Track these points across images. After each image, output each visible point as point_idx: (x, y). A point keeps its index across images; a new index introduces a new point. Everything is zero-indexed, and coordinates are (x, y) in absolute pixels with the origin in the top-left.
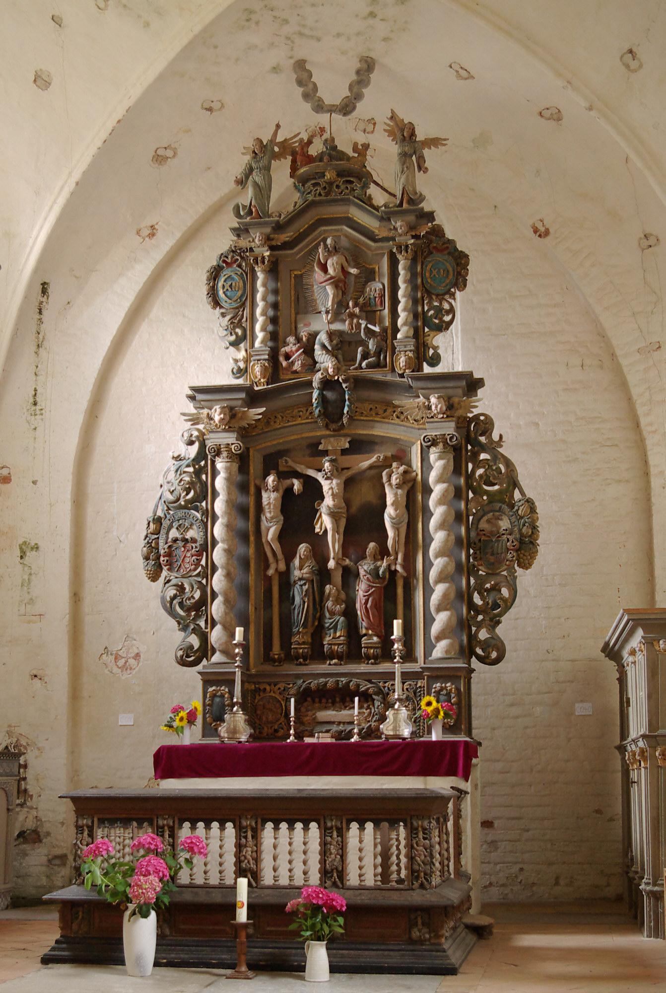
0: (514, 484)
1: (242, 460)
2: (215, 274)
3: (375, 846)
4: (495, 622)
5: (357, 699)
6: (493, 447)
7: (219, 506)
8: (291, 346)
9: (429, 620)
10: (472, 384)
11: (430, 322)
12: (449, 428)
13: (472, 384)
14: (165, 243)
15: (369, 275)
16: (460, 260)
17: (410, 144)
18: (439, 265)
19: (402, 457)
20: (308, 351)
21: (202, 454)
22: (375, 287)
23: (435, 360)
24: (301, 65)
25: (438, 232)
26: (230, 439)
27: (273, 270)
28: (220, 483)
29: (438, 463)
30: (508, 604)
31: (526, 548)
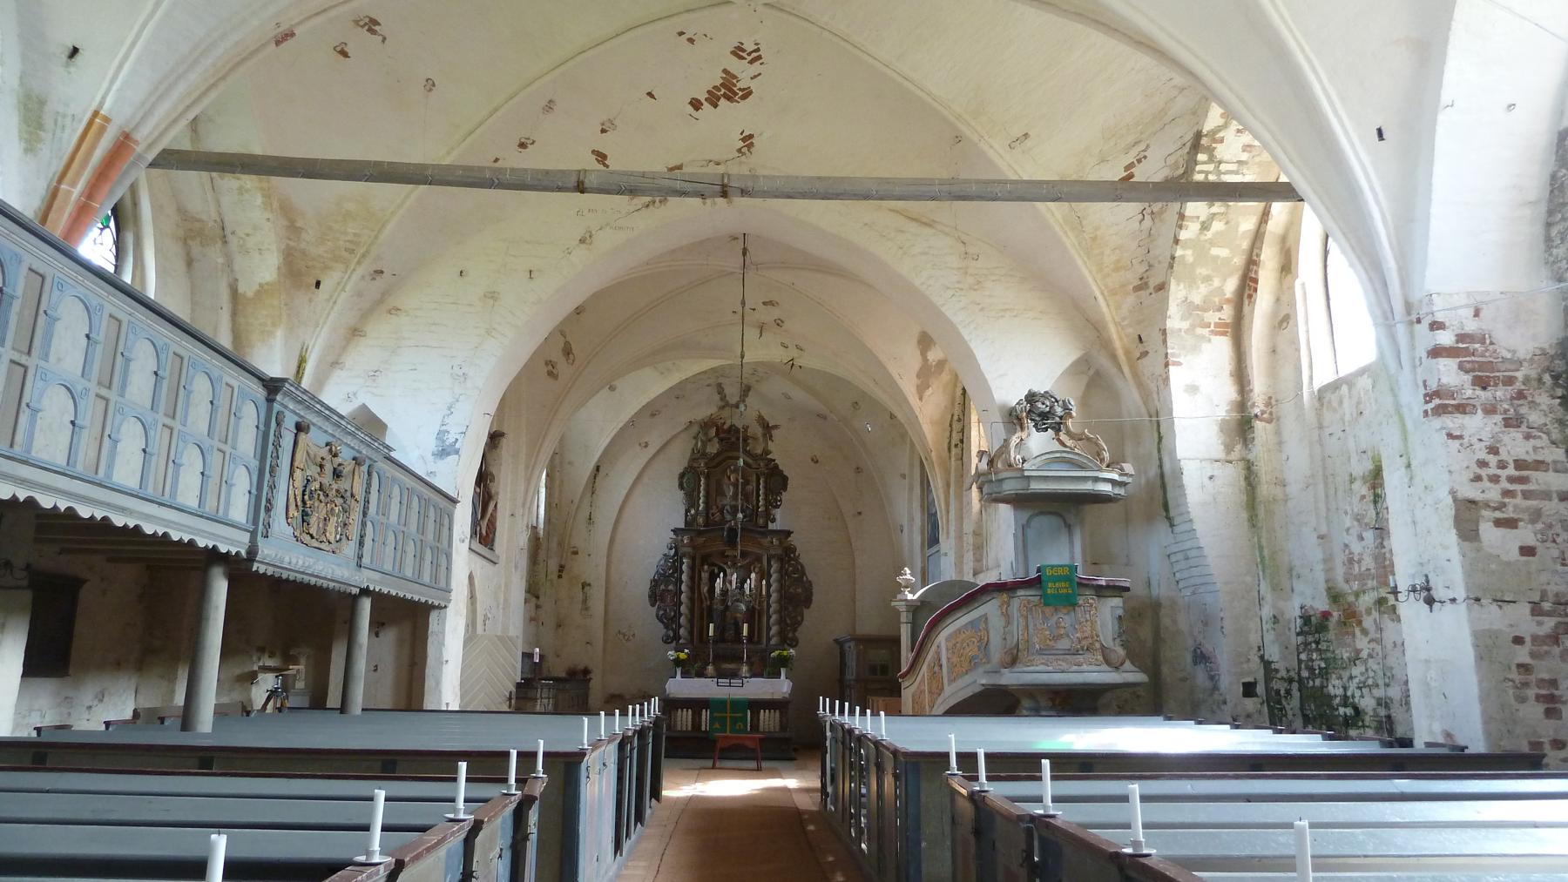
0: (804, 574)
1: (693, 559)
2: (682, 476)
3: (978, 182)
4: (795, 630)
5: (463, 766)
6: (796, 559)
7: (684, 577)
8: (714, 510)
9: (769, 629)
10: (789, 533)
11: (773, 503)
12: (779, 552)
13: (789, 533)
14: (652, 450)
15: (747, 482)
16: (785, 479)
17: (768, 429)
18: (776, 481)
19: (759, 559)
20: (722, 513)
21: (676, 553)
22: (750, 487)
23: (773, 521)
24: (719, 385)
25: (776, 466)
26: (689, 550)
27: (708, 477)
28: (684, 567)
29: (775, 566)
30: (800, 623)
31: (808, 601)
